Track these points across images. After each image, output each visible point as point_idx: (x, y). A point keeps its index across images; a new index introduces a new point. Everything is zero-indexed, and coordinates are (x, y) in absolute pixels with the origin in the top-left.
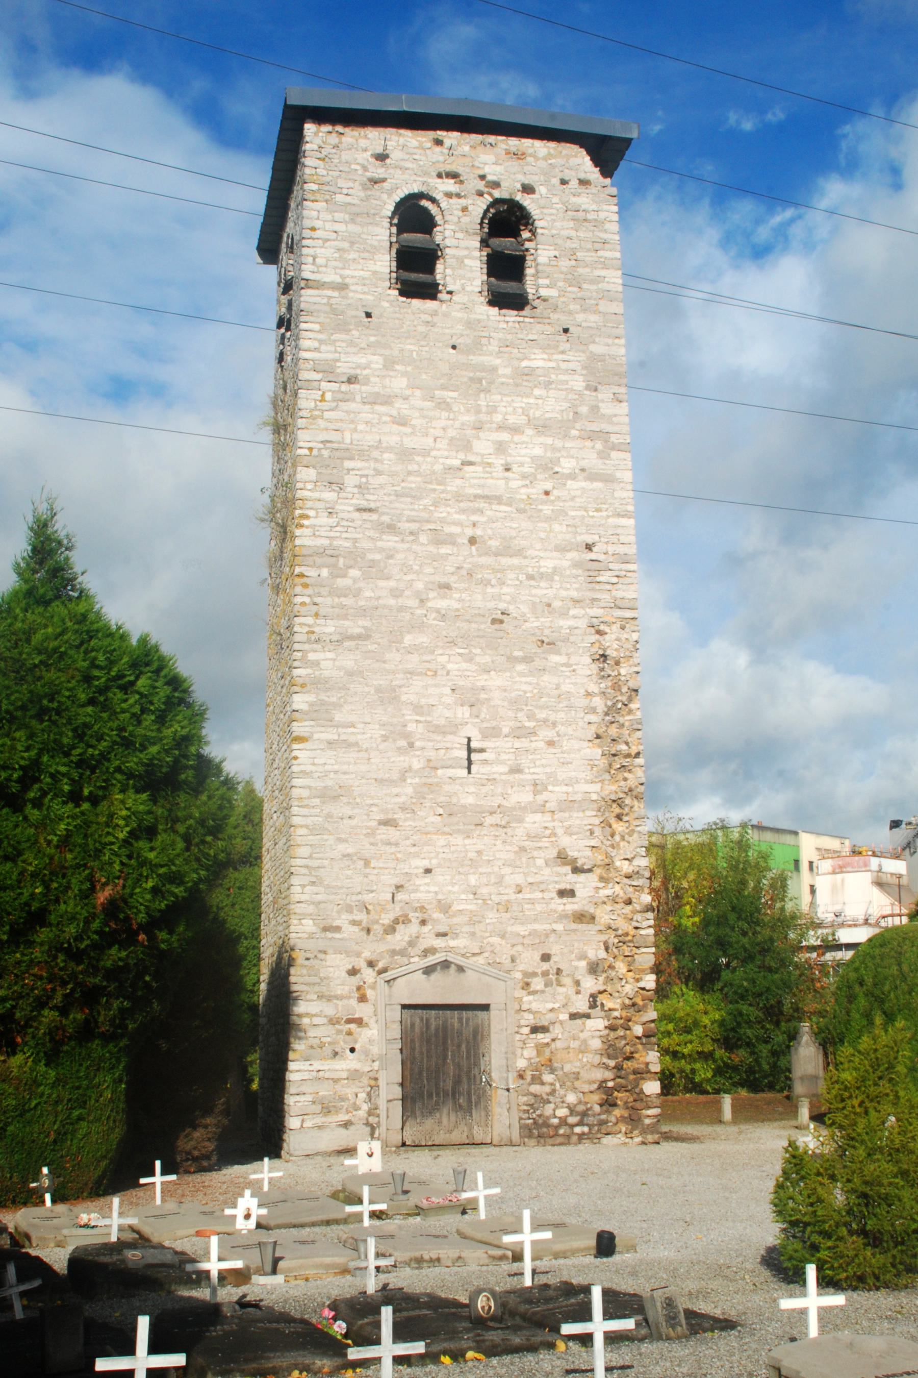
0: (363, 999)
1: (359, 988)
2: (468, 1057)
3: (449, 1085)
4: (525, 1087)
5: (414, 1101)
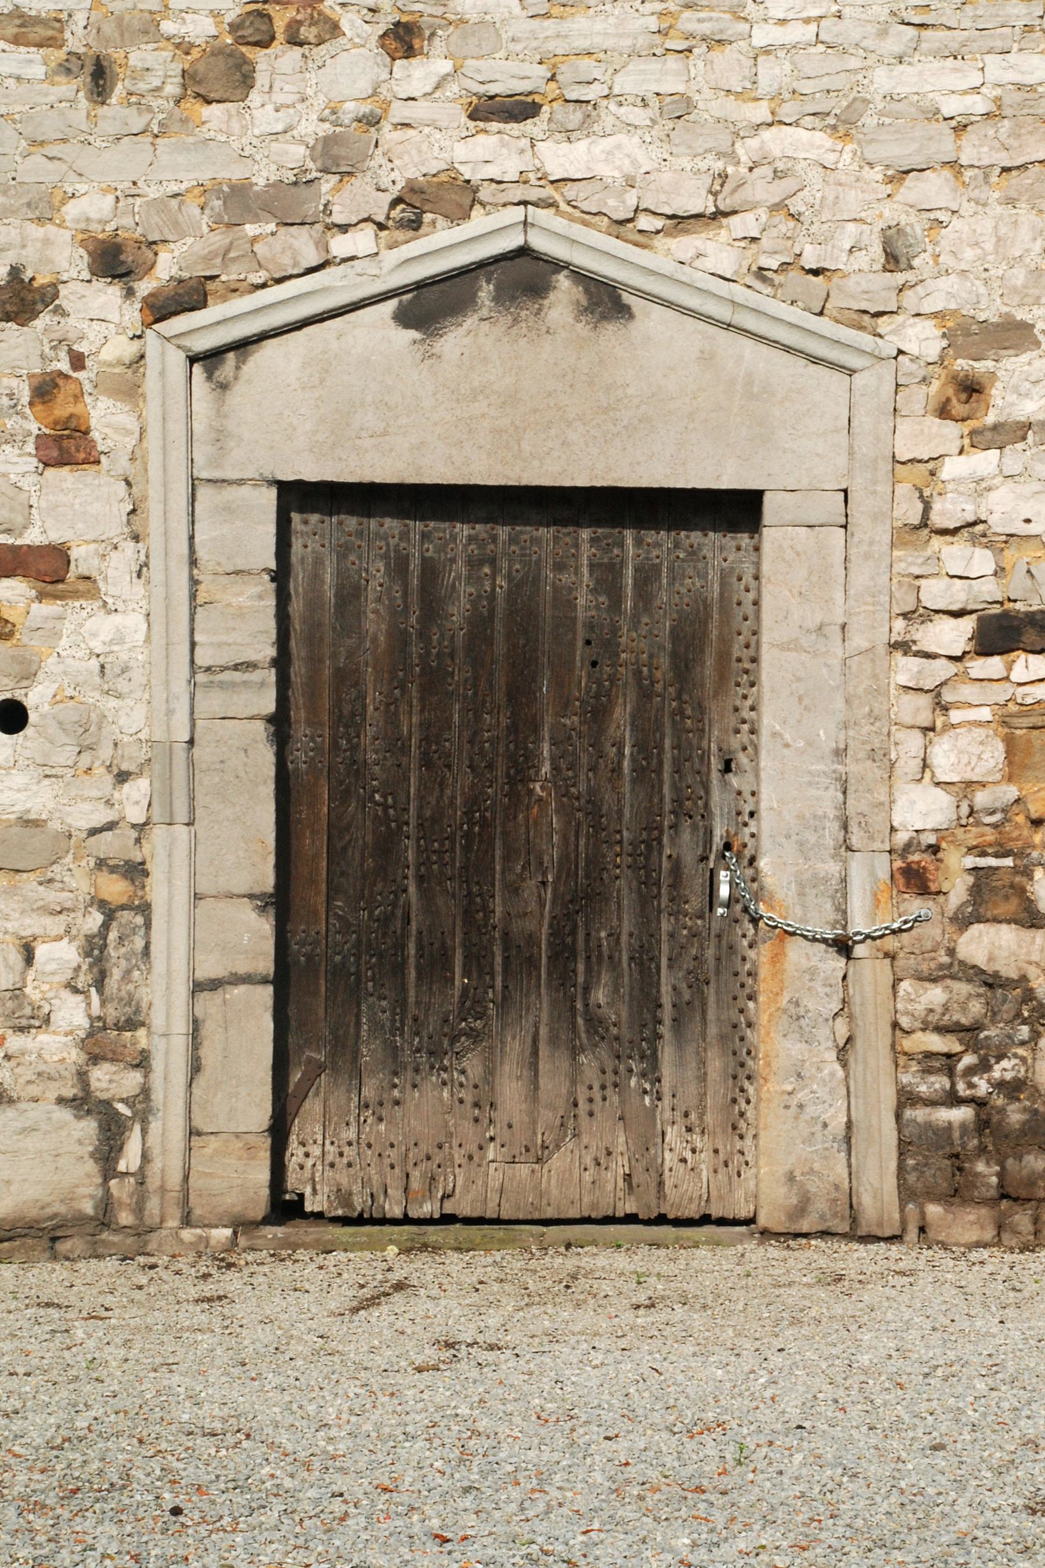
0: (67, 446)
1: (45, 390)
2: (646, 773)
3: (530, 907)
4: (933, 932)
5: (348, 988)
